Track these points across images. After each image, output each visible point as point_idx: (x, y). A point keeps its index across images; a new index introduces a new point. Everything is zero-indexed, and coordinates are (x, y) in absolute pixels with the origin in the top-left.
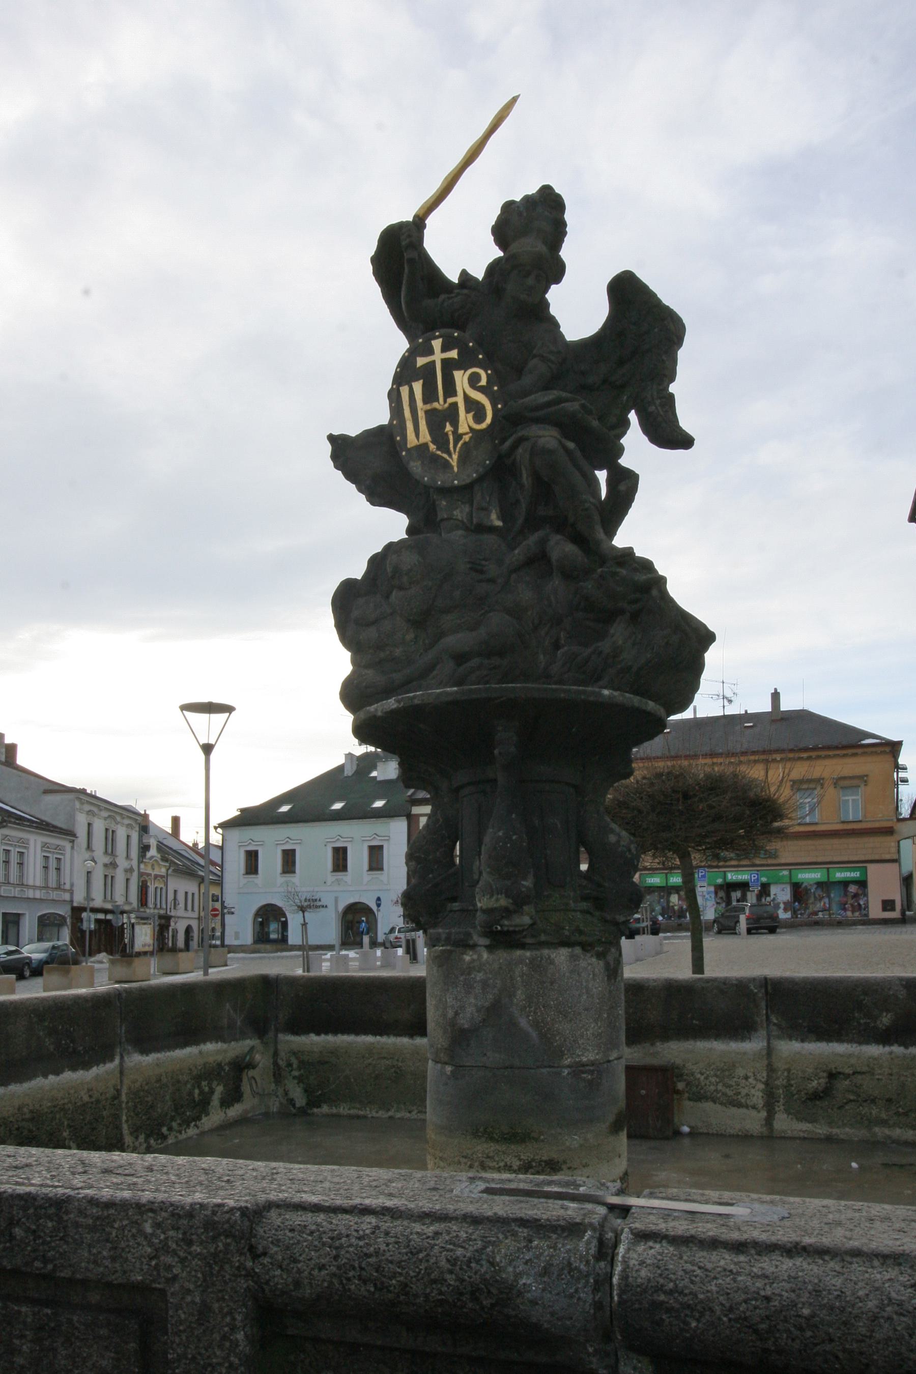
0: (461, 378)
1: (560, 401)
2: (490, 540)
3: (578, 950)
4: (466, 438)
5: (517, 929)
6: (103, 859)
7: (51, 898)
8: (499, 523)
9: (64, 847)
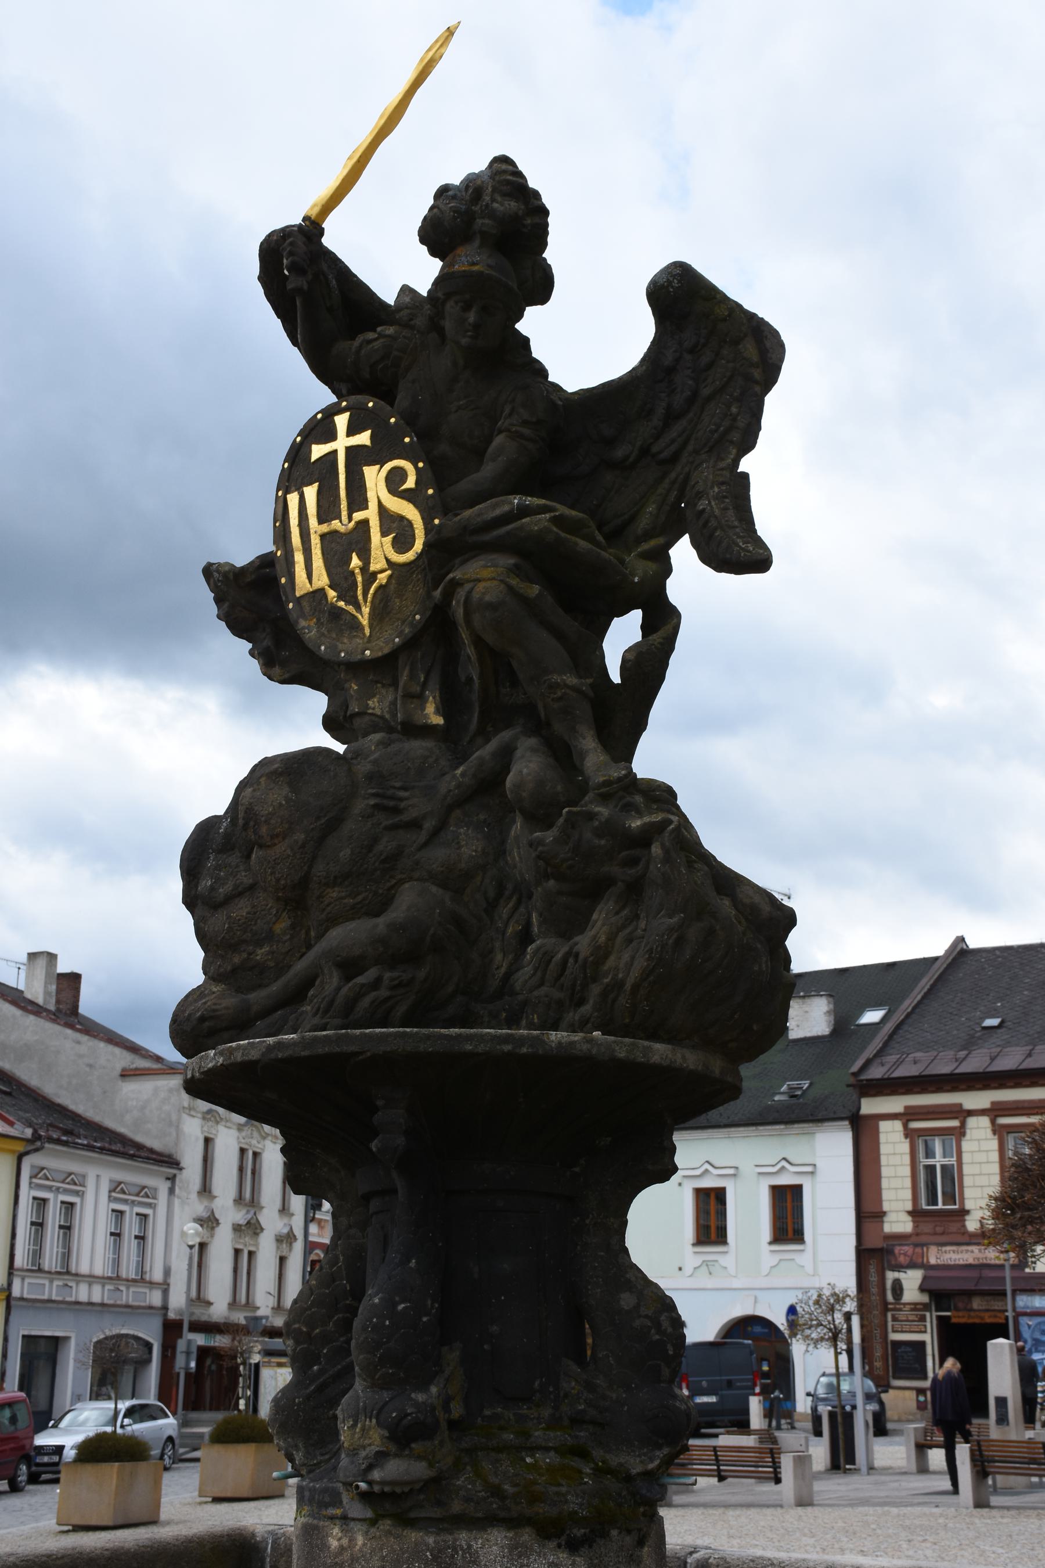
0: (374, 477)
1: (524, 511)
2: (418, 747)
3: (527, 1535)
4: (383, 578)
5: (398, 1490)
6: (229, 1215)
7: (124, 1302)
8: (438, 720)
9: (156, 1189)
